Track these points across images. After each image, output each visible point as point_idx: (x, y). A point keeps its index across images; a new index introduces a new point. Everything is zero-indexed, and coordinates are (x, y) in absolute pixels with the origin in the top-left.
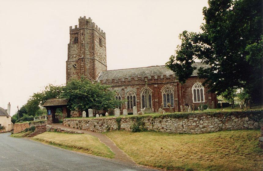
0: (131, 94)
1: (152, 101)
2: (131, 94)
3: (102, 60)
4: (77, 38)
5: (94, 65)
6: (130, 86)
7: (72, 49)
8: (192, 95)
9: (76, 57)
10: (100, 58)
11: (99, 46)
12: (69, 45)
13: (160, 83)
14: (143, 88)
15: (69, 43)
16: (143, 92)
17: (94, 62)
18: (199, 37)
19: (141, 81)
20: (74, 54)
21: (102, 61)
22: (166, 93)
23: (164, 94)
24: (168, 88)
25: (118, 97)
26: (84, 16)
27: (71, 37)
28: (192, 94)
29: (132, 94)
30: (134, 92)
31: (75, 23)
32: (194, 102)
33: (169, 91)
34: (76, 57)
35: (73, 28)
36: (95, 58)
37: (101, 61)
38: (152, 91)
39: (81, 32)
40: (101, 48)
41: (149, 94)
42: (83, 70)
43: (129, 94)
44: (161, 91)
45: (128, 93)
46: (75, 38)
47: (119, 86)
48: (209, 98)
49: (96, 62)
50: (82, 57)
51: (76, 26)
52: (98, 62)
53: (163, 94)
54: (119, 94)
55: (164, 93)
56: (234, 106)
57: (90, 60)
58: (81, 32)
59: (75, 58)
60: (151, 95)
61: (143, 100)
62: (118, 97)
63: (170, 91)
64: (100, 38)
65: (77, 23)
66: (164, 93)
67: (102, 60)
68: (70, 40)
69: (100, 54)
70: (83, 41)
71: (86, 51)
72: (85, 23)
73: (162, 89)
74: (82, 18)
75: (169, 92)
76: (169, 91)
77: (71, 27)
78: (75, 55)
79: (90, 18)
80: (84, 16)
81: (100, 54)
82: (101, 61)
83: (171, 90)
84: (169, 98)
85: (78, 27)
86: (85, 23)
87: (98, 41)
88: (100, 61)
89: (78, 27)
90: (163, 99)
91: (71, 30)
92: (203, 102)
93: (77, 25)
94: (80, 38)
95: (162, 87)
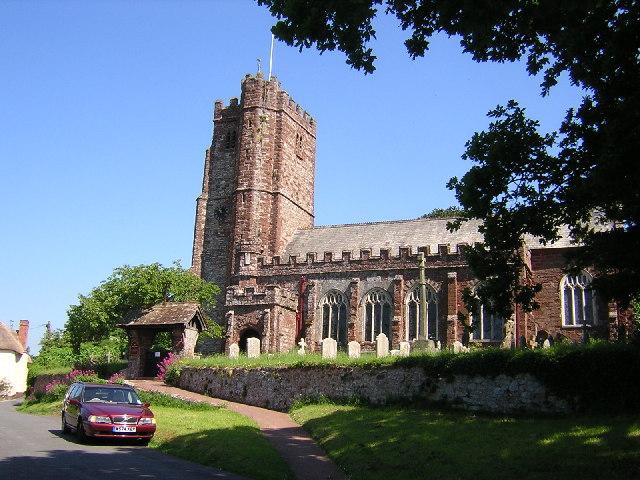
3: (300, 197)
5: (275, 211)
18: (594, 104)
26: (449, 186)
31: (230, 93)
32: (564, 324)
35: (226, 104)
36: (281, 191)
37: (298, 199)
51: (481, 229)
52: (287, 201)
56: (313, 263)
68: (215, 137)
71: (256, 172)
80: (449, 186)
82: (298, 199)
87: (292, 142)
88: (294, 199)
91: (219, 112)
92: (340, 285)
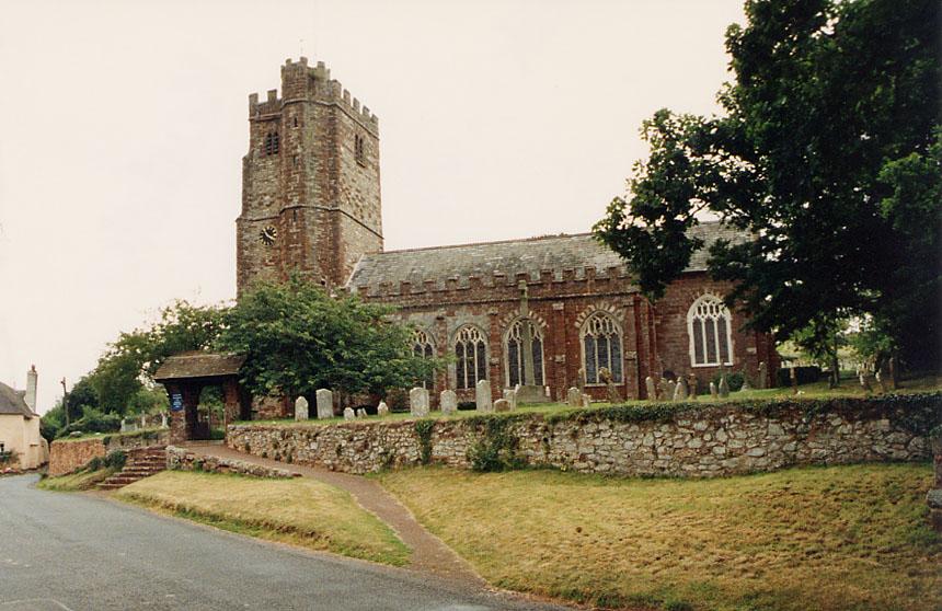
0: (470, 336)
1: (543, 362)
2: (470, 336)
4: (276, 134)
6: (464, 307)
7: (259, 175)
8: (688, 340)
9: (272, 203)
10: (358, 206)
11: (353, 163)
12: (247, 161)
13: (572, 298)
14: (511, 315)
15: (246, 152)
16: (511, 329)
17: (335, 221)
19: (504, 291)
20: (265, 195)
21: (365, 219)
22: (594, 334)
23: (588, 338)
24: (601, 316)
25: (423, 347)
26: (302, 58)
27: (255, 132)
28: (688, 336)
29: (473, 334)
30: (480, 328)
31: (269, 82)
33: (604, 324)
34: (272, 203)
36: (341, 207)
37: (362, 217)
38: (544, 324)
39: (291, 115)
40: (360, 172)
41: (535, 334)
42: (299, 251)
43: (462, 335)
44: (577, 324)
45: (459, 334)
46: (269, 136)
47: (426, 308)
48: (750, 350)
49: (345, 222)
50: (292, 205)
51: (273, 93)
53: (582, 335)
54: (425, 337)
55: (589, 332)
57: (322, 215)
58: (291, 115)
59: (268, 206)
60: (541, 340)
61: (513, 358)
62: (423, 347)
63: (610, 324)
64: (357, 137)
65: (277, 83)
66: (589, 332)
67: (366, 215)
69: (359, 192)
70: (296, 147)
72: (304, 81)
73: (581, 317)
74: (295, 65)
75: (605, 329)
76: (604, 324)
77: (254, 97)
78: (267, 198)
79: (321, 65)
80: (302, 58)
81: (359, 192)
82: (362, 217)
83: (613, 321)
84: (606, 351)
85: (279, 96)
86: (304, 81)
88: (358, 217)
89: (279, 96)
90: (583, 355)
93: (275, 91)
94: (288, 136)
95: (579, 312)
